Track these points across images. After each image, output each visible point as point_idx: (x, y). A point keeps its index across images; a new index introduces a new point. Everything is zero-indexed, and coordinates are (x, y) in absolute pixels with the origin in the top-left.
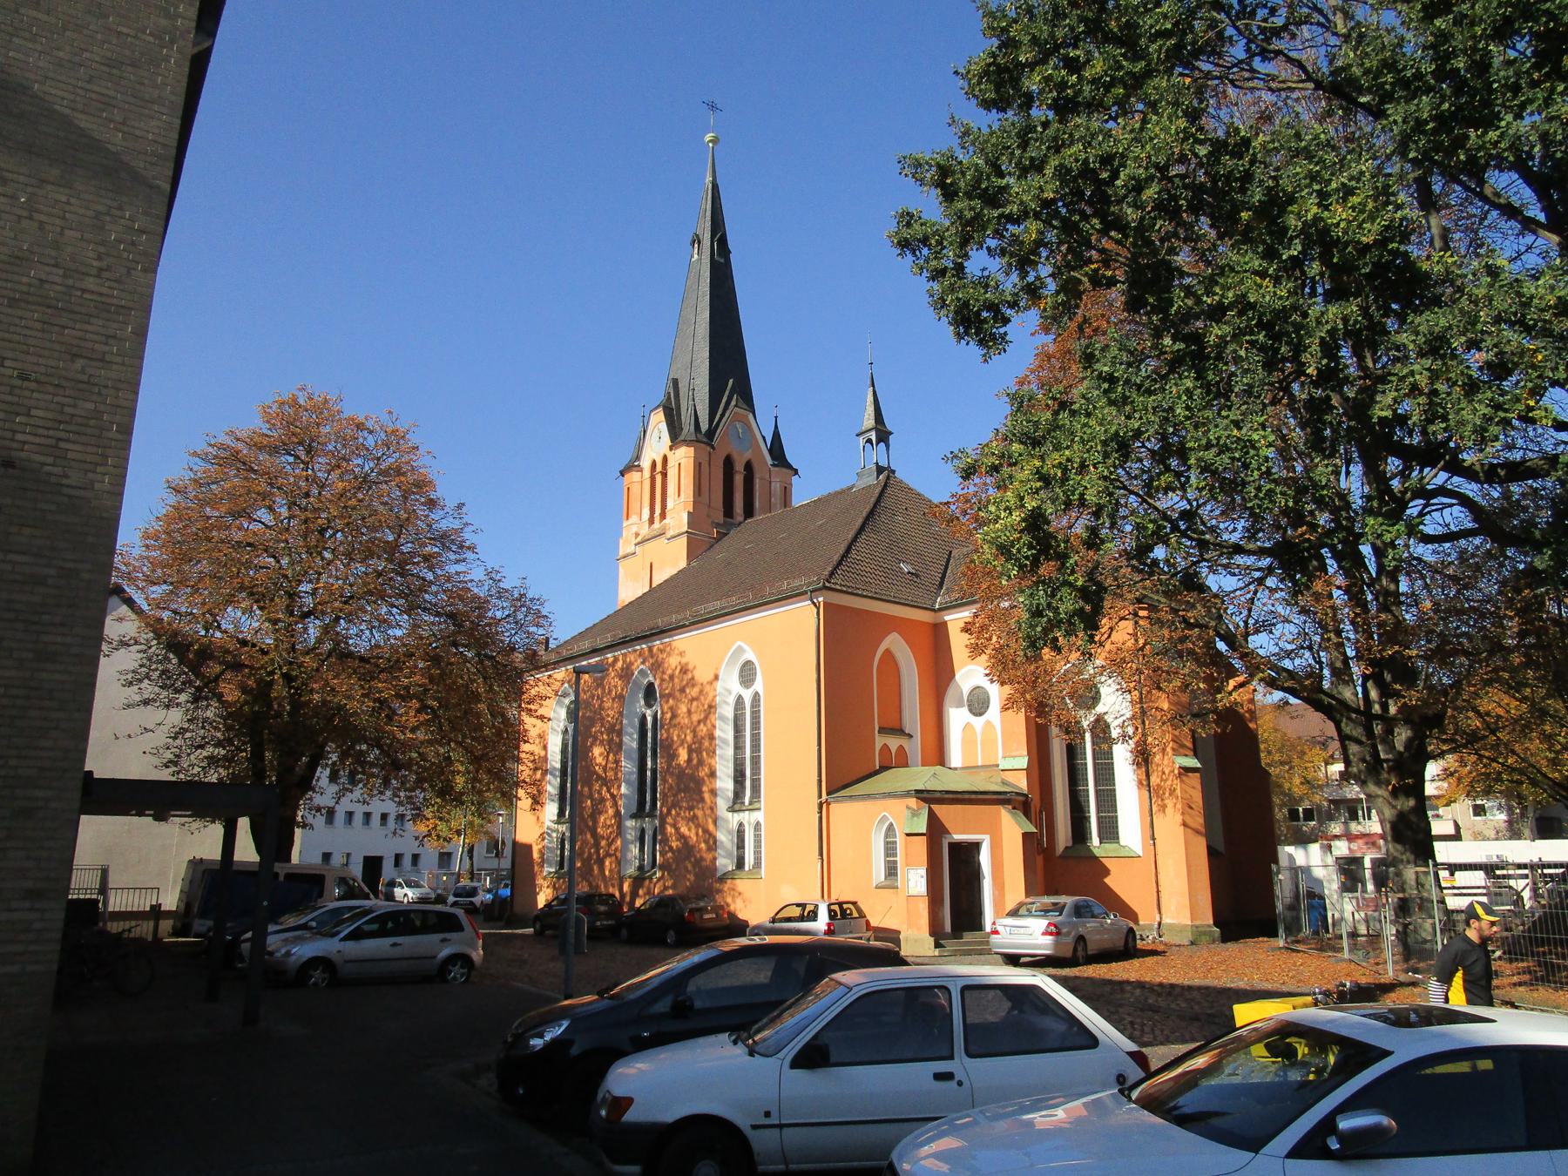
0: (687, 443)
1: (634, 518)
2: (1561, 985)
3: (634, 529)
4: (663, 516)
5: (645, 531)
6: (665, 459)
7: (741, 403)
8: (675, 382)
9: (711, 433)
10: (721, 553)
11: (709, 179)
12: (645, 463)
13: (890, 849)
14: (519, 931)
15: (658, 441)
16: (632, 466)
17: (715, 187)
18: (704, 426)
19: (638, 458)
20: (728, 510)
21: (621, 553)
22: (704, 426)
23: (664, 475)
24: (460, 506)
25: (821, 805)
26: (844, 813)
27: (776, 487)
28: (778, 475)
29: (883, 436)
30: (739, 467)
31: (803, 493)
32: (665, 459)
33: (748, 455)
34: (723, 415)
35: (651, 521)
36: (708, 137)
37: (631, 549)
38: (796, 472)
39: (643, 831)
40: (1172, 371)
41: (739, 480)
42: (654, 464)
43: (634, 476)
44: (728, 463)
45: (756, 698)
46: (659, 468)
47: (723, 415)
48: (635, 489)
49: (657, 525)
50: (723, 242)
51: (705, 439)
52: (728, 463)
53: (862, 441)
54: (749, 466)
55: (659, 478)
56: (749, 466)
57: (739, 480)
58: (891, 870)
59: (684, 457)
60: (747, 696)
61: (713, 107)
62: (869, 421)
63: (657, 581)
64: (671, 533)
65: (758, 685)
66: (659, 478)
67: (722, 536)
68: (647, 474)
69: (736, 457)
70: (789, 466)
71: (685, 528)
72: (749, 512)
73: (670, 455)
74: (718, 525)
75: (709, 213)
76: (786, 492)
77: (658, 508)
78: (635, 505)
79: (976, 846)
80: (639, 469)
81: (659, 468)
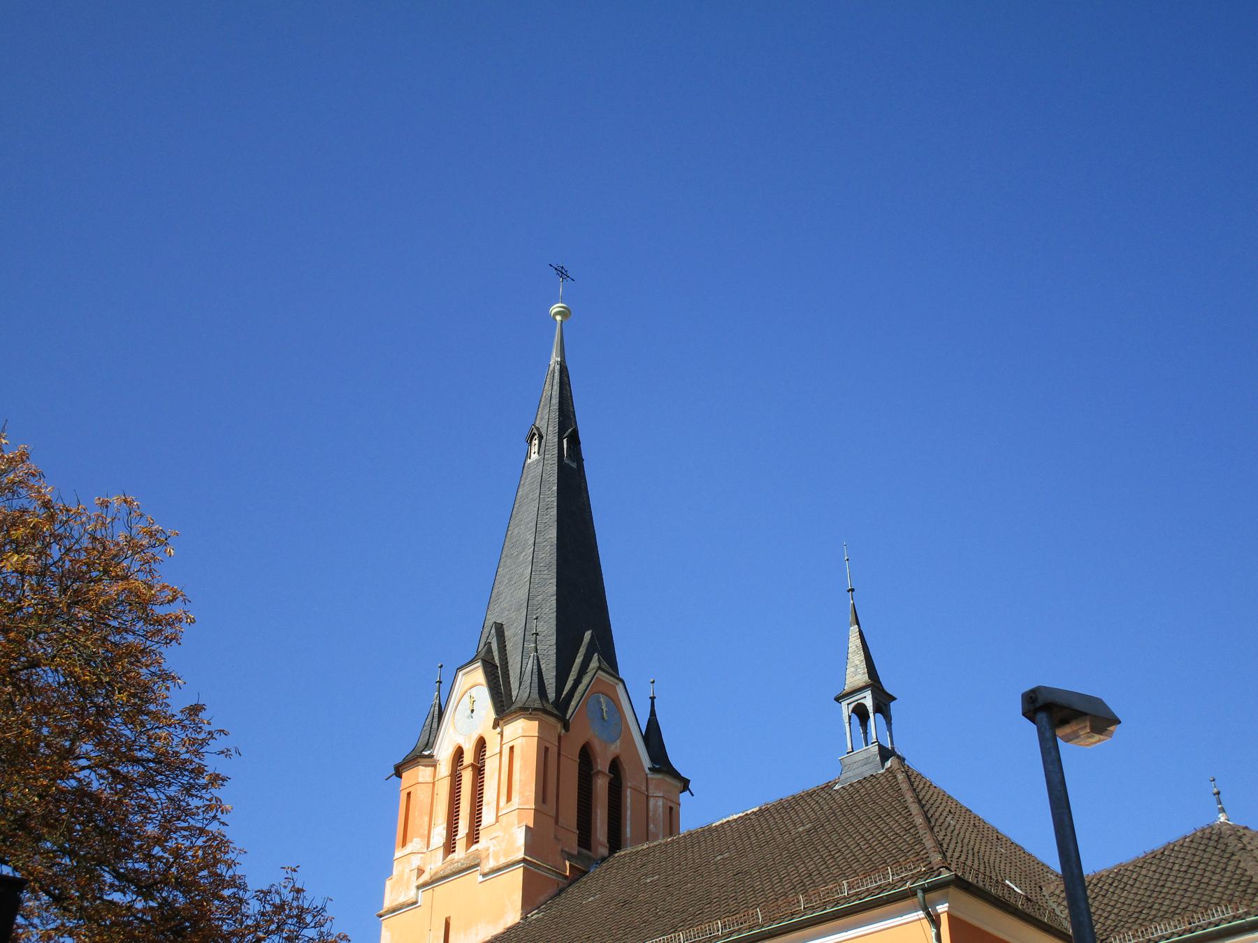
0: (526, 711)
1: (415, 844)
3: (416, 861)
4: (473, 837)
5: (436, 863)
6: (481, 744)
7: (605, 665)
8: (500, 629)
9: (561, 705)
10: (592, 895)
11: (555, 358)
12: (443, 752)
15: (469, 712)
16: (420, 755)
17: (564, 370)
18: (552, 695)
19: (429, 744)
20: (585, 838)
21: (388, 903)
22: (552, 695)
23: (479, 770)
24: (195, 710)
27: (657, 805)
28: (659, 787)
29: (883, 702)
30: (602, 764)
31: (695, 814)
32: (481, 744)
33: (615, 748)
34: (577, 682)
35: (450, 847)
36: (555, 308)
37: (411, 894)
38: (685, 785)
41: (601, 785)
42: (459, 753)
43: (422, 773)
44: (586, 755)
46: (468, 758)
47: (577, 682)
48: (421, 795)
49: (460, 853)
50: (574, 440)
51: (553, 709)
52: (586, 755)
53: (846, 708)
54: (615, 766)
55: (467, 777)
56: (615, 766)
57: (601, 785)
59: (523, 733)
61: (562, 272)
62: (856, 674)
64: (491, 864)
66: (467, 777)
67: (579, 874)
68: (444, 769)
69: (597, 747)
70: (675, 774)
71: (520, 855)
72: (615, 842)
74: (570, 857)
75: (555, 401)
76: (672, 813)
77: (464, 819)
78: (418, 820)
80: (432, 762)
81: (468, 758)
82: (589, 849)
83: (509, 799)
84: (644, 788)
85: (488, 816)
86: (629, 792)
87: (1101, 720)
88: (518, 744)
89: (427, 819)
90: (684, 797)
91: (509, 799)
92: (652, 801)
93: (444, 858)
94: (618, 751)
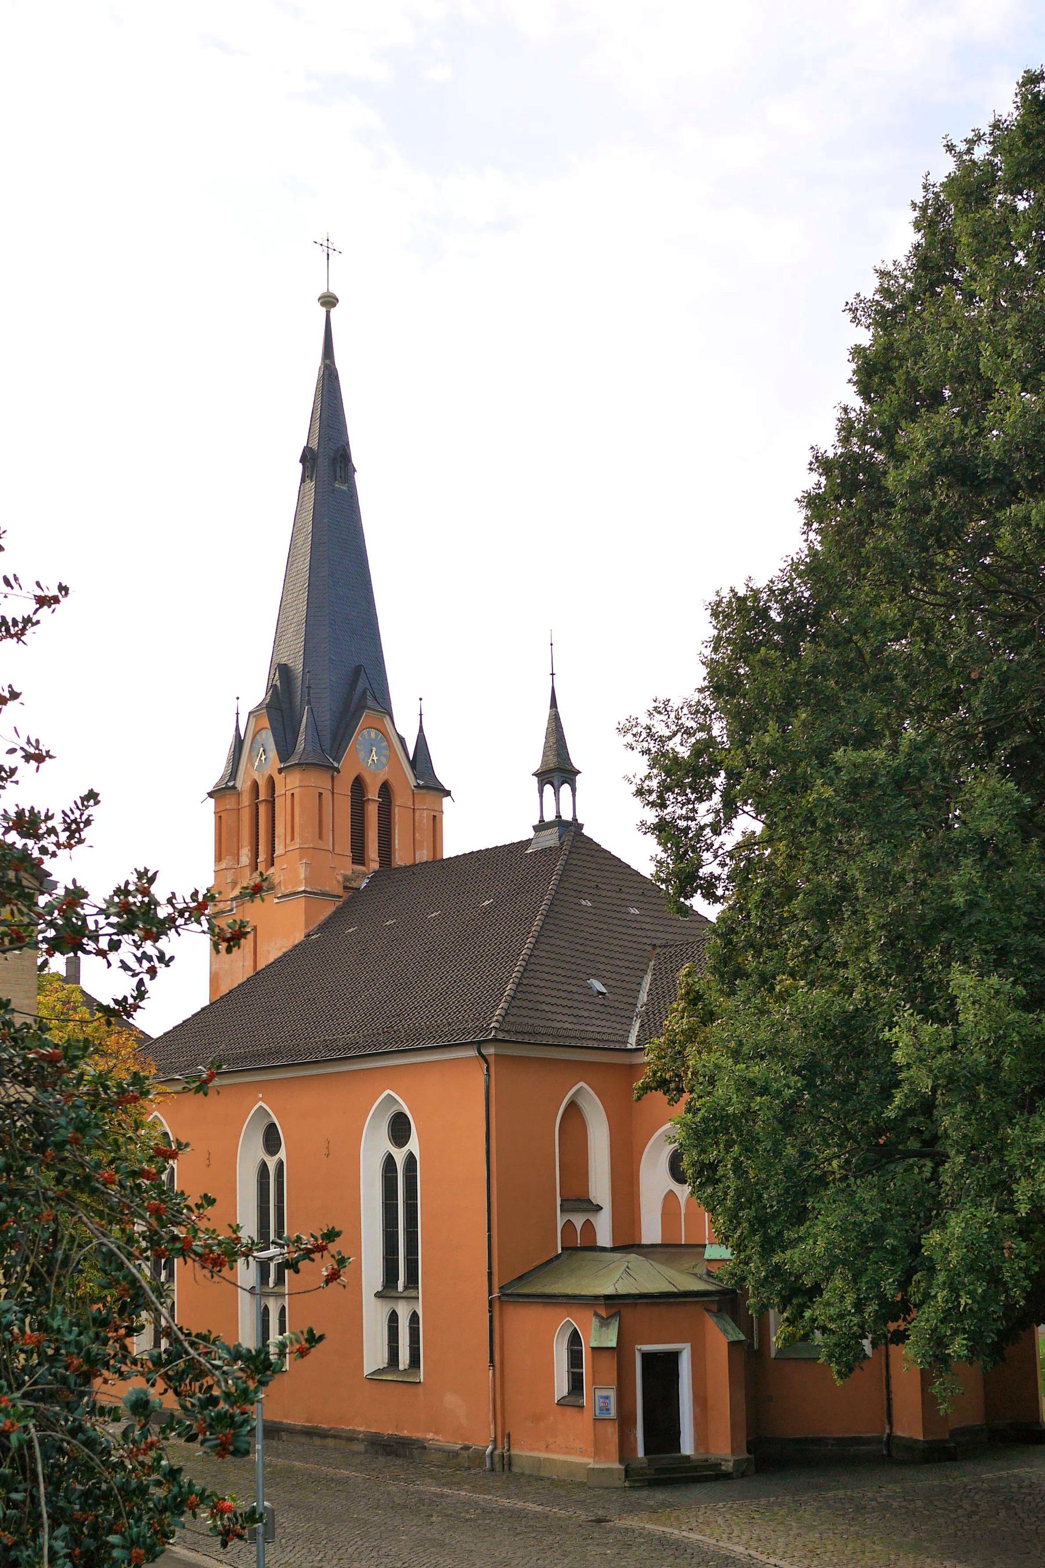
2: (1042, 1443)
6: (271, 783)
13: (575, 1359)
14: (683, 1212)
25: (491, 1302)
26: (523, 1321)
30: (373, 794)
38: (448, 793)
39: (393, 1318)
40: (659, 1086)
41: (372, 812)
42: (255, 785)
44: (359, 785)
45: (411, 1159)
52: (359, 785)
54: (386, 789)
55: (262, 809)
56: (386, 789)
58: (576, 1384)
60: (399, 1156)
63: (261, 965)
65: (413, 1145)
66: (262, 809)
68: (246, 800)
69: (368, 779)
73: (278, 779)
79: (673, 1357)
82: (363, 864)
83: (293, 839)
84: (410, 804)
85: (279, 850)
86: (396, 809)
87: (311, 1331)
88: (296, 791)
89: (235, 840)
90: (446, 801)
91: (293, 839)
92: (417, 813)
93: (251, 875)
94: (385, 778)
